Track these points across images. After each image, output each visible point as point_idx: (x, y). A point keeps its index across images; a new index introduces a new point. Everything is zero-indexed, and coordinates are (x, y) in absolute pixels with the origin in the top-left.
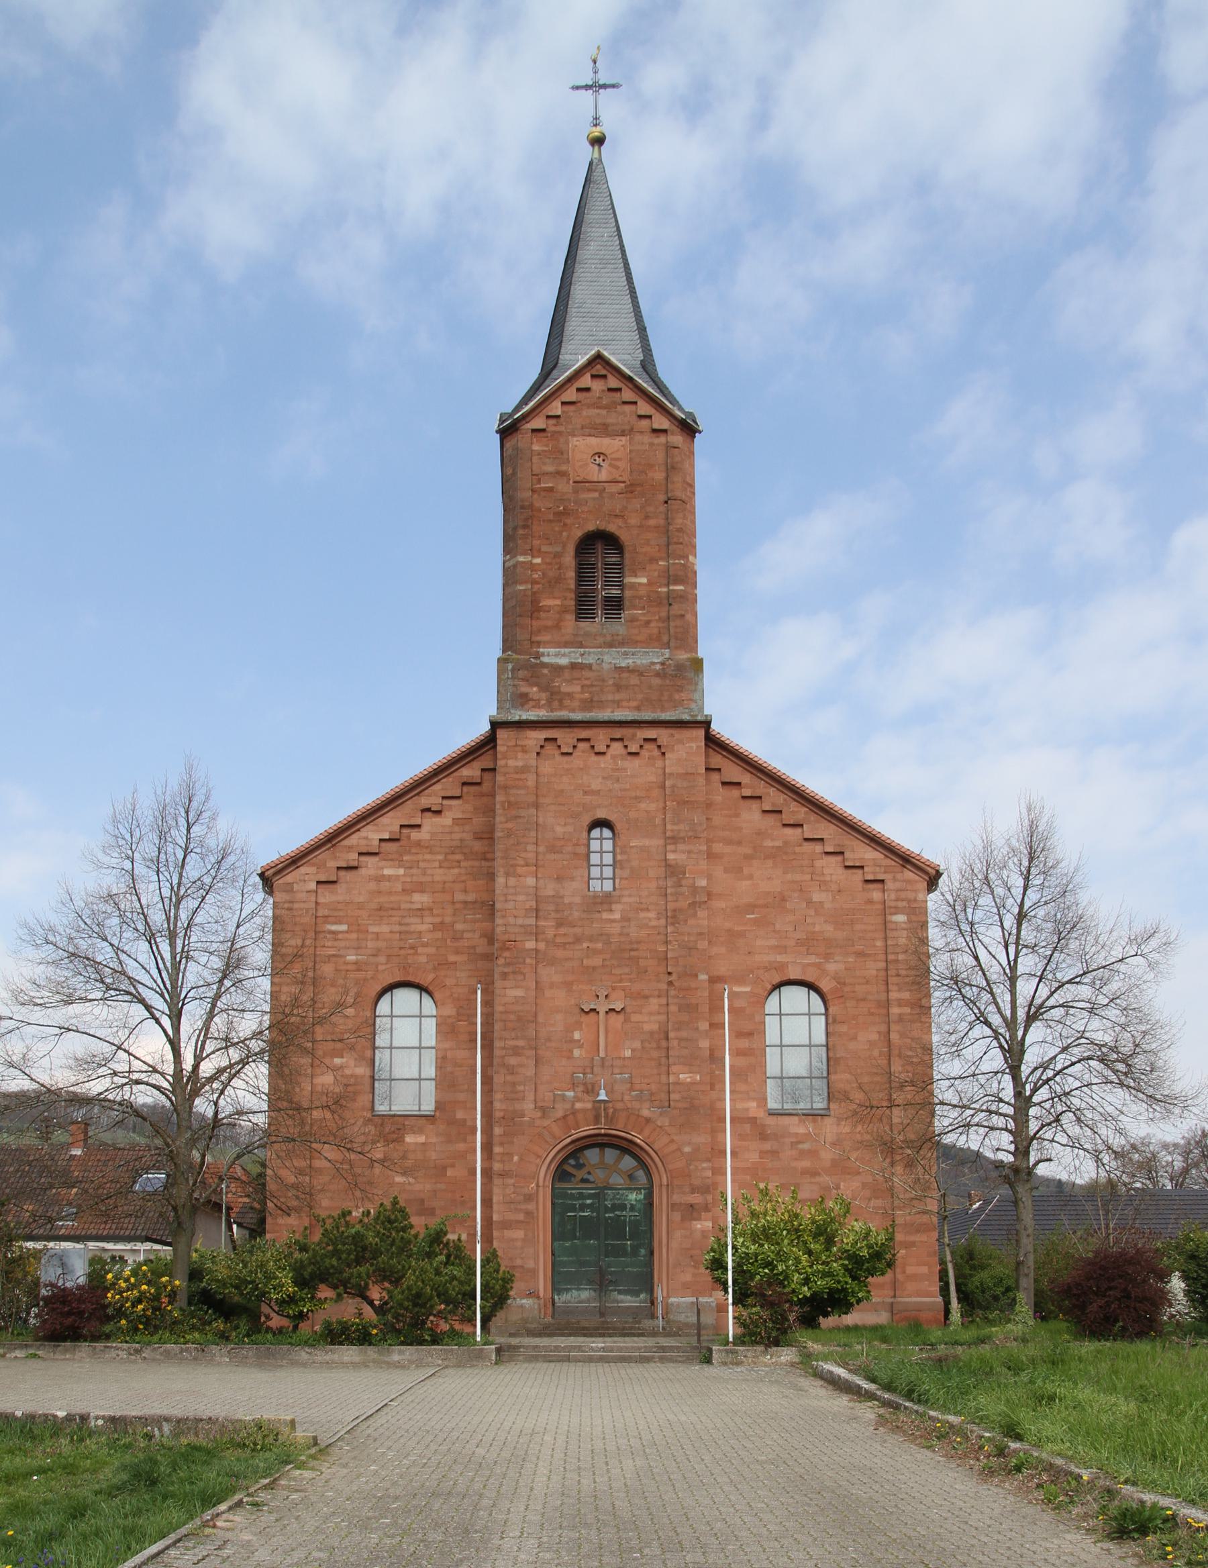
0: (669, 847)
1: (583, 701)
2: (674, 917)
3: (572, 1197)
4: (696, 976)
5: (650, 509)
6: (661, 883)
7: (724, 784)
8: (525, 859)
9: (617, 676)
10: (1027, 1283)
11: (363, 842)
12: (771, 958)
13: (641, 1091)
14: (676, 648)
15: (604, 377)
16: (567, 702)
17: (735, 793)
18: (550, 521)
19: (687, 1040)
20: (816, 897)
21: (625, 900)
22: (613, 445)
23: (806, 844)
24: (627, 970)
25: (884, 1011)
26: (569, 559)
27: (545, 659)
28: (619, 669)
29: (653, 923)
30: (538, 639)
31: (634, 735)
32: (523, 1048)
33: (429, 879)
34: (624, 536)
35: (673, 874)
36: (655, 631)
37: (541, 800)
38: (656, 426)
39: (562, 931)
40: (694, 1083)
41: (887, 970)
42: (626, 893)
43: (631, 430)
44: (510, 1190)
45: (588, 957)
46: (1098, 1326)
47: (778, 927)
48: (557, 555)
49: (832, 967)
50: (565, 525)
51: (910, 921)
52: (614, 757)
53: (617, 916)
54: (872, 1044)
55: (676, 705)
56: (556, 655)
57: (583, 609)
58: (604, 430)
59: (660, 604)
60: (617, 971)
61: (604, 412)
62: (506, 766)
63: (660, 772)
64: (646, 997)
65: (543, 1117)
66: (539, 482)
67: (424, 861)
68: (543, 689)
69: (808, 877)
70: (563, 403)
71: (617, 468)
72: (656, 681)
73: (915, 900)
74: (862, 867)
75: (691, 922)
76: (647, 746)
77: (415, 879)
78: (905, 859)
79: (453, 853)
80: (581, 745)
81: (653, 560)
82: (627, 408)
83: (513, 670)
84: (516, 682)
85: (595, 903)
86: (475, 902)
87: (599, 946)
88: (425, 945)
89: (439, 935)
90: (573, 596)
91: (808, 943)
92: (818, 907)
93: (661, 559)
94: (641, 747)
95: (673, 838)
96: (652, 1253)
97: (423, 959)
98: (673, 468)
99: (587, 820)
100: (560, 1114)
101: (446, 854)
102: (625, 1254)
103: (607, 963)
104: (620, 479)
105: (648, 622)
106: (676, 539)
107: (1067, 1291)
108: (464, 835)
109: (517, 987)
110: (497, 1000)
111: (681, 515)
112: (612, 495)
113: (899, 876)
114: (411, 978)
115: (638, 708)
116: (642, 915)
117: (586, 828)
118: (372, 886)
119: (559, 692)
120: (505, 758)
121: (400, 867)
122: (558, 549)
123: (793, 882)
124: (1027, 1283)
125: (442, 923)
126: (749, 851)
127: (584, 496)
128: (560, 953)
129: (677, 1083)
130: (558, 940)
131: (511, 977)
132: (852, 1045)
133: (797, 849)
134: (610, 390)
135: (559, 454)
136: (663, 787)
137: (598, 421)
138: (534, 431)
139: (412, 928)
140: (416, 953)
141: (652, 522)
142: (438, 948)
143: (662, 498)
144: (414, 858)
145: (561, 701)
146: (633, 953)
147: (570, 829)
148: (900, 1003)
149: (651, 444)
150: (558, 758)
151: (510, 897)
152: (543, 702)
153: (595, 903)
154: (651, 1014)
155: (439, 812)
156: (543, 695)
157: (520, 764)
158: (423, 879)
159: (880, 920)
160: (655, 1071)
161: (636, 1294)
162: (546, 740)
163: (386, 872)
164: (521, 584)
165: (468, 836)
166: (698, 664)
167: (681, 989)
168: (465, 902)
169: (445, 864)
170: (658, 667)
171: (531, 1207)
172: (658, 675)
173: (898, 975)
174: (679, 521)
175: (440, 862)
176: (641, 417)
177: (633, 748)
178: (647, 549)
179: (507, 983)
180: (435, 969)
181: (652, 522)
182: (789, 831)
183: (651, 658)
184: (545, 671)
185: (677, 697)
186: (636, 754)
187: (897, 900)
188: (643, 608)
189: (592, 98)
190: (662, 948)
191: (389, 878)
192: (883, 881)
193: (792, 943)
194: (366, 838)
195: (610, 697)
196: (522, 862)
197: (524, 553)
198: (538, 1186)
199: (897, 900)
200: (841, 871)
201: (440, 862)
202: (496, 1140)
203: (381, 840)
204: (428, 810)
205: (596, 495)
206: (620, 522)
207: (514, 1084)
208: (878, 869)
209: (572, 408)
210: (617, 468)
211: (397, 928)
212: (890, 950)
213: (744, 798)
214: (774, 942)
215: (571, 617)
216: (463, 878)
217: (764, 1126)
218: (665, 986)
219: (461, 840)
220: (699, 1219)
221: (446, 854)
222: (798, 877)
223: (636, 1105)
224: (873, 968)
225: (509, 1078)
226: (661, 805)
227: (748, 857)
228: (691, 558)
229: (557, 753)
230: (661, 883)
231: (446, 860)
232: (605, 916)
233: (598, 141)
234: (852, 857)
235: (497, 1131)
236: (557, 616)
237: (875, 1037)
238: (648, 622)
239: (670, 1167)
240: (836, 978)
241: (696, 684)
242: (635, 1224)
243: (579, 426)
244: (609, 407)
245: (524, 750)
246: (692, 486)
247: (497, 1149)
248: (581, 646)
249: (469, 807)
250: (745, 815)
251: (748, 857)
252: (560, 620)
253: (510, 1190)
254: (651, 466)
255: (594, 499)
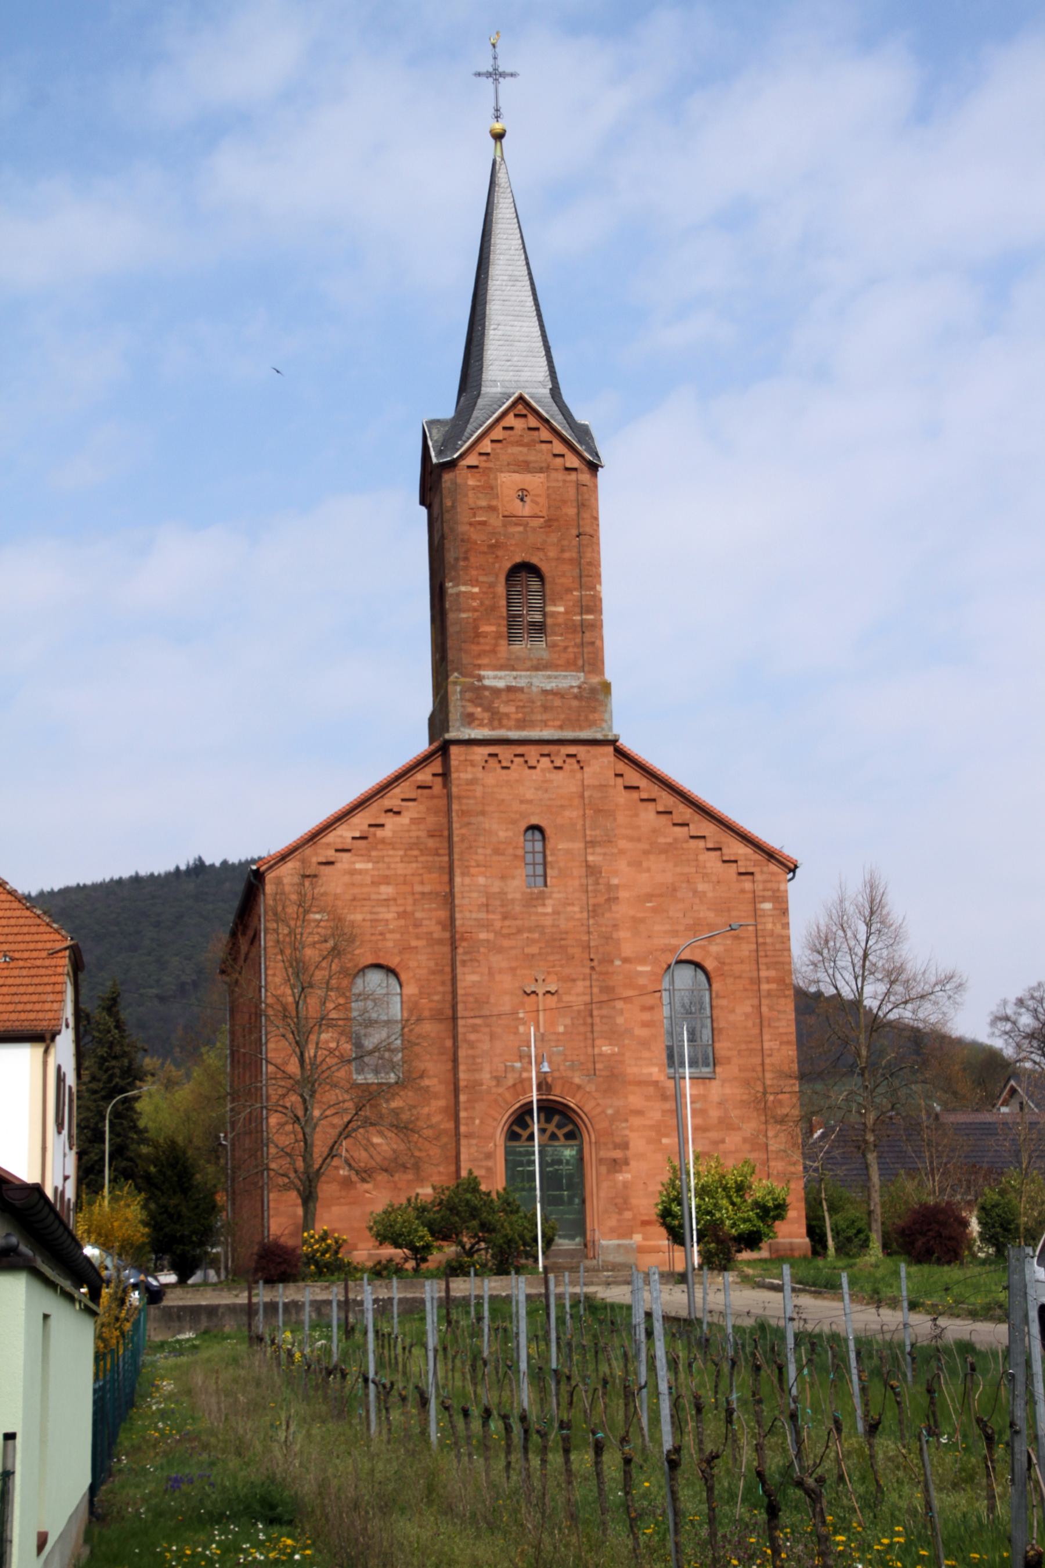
0: (589, 850)
1: (518, 720)
2: (594, 911)
3: (520, 1154)
4: (612, 962)
5: (565, 543)
6: (584, 881)
7: (626, 788)
8: (476, 861)
9: (543, 698)
10: (877, 1226)
11: (339, 840)
12: (666, 941)
13: (573, 1061)
14: (589, 672)
15: (525, 416)
16: (505, 722)
17: (635, 795)
18: (484, 553)
19: (606, 1017)
20: (701, 887)
21: (555, 896)
22: (534, 481)
23: (691, 841)
24: (557, 957)
25: (756, 987)
26: (501, 589)
27: (487, 682)
28: (545, 692)
29: (578, 916)
30: (479, 662)
31: (559, 751)
32: (480, 1026)
33: (392, 872)
34: (544, 568)
35: (592, 874)
36: (572, 656)
37: (487, 808)
38: (568, 465)
39: (507, 923)
40: (613, 1055)
41: (757, 951)
42: (556, 889)
43: (548, 467)
44: (473, 1149)
45: (528, 946)
46: (920, 1256)
47: (671, 914)
48: (492, 585)
49: (714, 949)
50: (497, 557)
51: (774, 909)
52: (543, 770)
53: (549, 910)
54: (747, 1016)
55: (592, 724)
56: (495, 677)
57: (513, 627)
58: (525, 467)
59: (574, 631)
60: (551, 958)
61: (524, 450)
62: (459, 778)
63: (580, 783)
64: (574, 980)
65: (498, 1085)
66: (474, 515)
67: (388, 856)
68: (487, 709)
69: (693, 870)
70: (493, 441)
71: (537, 503)
72: (575, 703)
73: (778, 890)
74: (736, 861)
75: (607, 915)
76: (569, 760)
77: (381, 872)
78: (770, 855)
79: (411, 849)
80: (517, 760)
81: (569, 590)
82: (544, 446)
83: (461, 692)
84: (464, 703)
85: (532, 899)
86: (430, 893)
87: (536, 936)
88: (392, 932)
89: (402, 922)
90: (505, 622)
91: (695, 927)
92: (701, 896)
93: (575, 589)
94: (564, 762)
95: (591, 842)
96: (583, 1201)
97: (390, 944)
98: (583, 505)
99: (524, 825)
100: (510, 1082)
101: (406, 850)
102: (562, 1203)
103: (543, 951)
104: (541, 514)
105: (566, 648)
106: (586, 572)
107: (902, 1232)
108: (420, 833)
109: (474, 973)
110: (460, 984)
111: (590, 550)
112: (534, 529)
113: (765, 869)
114: (381, 962)
115: (561, 727)
116: (569, 909)
117: (522, 832)
118: (347, 879)
119: (498, 712)
120: (457, 771)
121: (369, 861)
122: (492, 579)
123: (682, 874)
124: (877, 1226)
125: (405, 912)
126: (646, 847)
127: (513, 529)
128: (506, 943)
129: (600, 1055)
130: (505, 931)
131: (469, 964)
132: (732, 1018)
133: (685, 845)
134: (530, 429)
135: (489, 489)
136: (582, 797)
137: (521, 458)
138: (469, 467)
139: (381, 916)
140: (384, 939)
141: (567, 555)
142: (402, 934)
143: (575, 532)
144: (380, 853)
145: (500, 720)
146: (563, 942)
147: (510, 834)
148: (768, 980)
149: (565, 481)
150: (499, 770)
151: (465, 895)
152: (486, 721)
153: (532, 899)
154: (578, 995)
155: (398, 813)
156: (486, 715)
157: (469, 776)
158: (387, 872)
159: (751, 907)
160: (582, 1044)
161: (572, 1237)
162: (490, 755)
163: (358, 866)
164: (464, 611)
165: (423, 834)
166: (606, 687)
167: (601, 973)
168: (423, 893)
169: (406, 859)
170: (576, 690)
171: (490, 1164)
172: (576, 697)
173: (766, 956)
174: (589, 555)
175: (402, 857)
176: (555, 455)
177: (558, 763)
178: (563, 580)
179: (466, 970)
180: (400, 952)
181: (567, 555)
182: (677, 829)
183: (569, 681)
184: (487, 693)
185: (591, 717)
186: (560, 768)
187: (764, 890)
188: (562, 635)
189: (492, 87)
190: (585, 938)
191: (360, 872)
192: (752, 874)
193: (682, 928)
194: (341, 836)
195: (539, 717)
196: (473, 863)
197: (465, 584)
198: (495, 1145)
199: (764, 890)
200: (720, 864)
201: (402, 857)
202: (462, 1105)
203: (354, 838)
204: (390, 811)
205: (521, 529)
206: (541, 555)
207: (474, 1057)
208: (748, 863)
209: (499, 445)
210: (537, 503)
211: (369, 917)
212: (760, 933)
213: (642, 800)
214: (668, 927)
215: (504, 642)
216: (421, 871)
217: (664, 1088)
218: (587, 971)
219: (418, 837)
220: (620, 1171)
221: (406, 850)
222: (686, 870)
223: (569, 1074)
224: (746, 949)
225: (470, 1052)
226: (581, 813)
227: (646, 853)
228: (598, 587)
229: (498, 766)
230: (584, 881)
231: (406, 855)
232: (540, 910)
233: (499, 136)
234: (729, 852)
235: (463, 1098)
236: (493, 642)
237: (749, 1009)
238: (566, 648)
239: (597, 1127)
240: (717, 958)
241: (606, 706)
242: (570, 1177)
243: (505, 463)
244: (530, 445)
245: (473, 764)
246: (596, 519)
247: (463, 1114)
248: (513, 669)
249: (422, 808)
250: (643, 815)
251: (646, 853)
252: (496, 645)
253: (473, 1149)
254: (564, 502)
255: (519, 532)
